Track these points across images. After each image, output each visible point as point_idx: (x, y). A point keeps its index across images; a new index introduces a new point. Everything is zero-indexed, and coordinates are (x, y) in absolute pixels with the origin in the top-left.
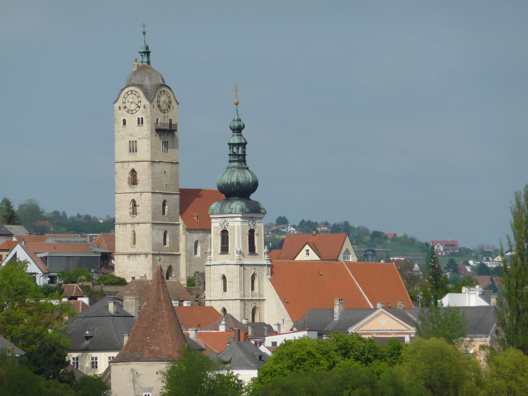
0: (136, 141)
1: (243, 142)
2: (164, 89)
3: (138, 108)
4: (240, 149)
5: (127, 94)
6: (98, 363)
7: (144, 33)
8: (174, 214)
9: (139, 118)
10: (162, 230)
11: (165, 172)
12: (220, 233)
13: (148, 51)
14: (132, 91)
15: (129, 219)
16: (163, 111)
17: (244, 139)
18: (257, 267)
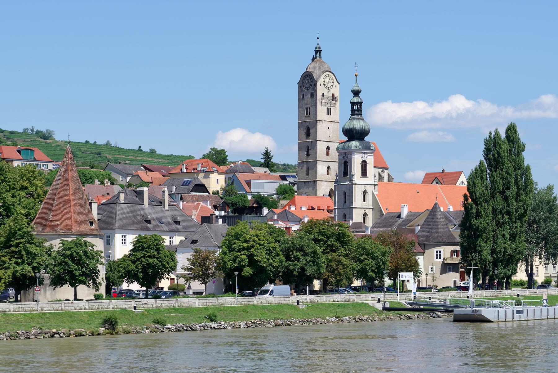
6: (121, 243)
7: (318, 39)
13: (320, 49)
14: (328, 75)
15: (325, 158)
17: (361, 99)
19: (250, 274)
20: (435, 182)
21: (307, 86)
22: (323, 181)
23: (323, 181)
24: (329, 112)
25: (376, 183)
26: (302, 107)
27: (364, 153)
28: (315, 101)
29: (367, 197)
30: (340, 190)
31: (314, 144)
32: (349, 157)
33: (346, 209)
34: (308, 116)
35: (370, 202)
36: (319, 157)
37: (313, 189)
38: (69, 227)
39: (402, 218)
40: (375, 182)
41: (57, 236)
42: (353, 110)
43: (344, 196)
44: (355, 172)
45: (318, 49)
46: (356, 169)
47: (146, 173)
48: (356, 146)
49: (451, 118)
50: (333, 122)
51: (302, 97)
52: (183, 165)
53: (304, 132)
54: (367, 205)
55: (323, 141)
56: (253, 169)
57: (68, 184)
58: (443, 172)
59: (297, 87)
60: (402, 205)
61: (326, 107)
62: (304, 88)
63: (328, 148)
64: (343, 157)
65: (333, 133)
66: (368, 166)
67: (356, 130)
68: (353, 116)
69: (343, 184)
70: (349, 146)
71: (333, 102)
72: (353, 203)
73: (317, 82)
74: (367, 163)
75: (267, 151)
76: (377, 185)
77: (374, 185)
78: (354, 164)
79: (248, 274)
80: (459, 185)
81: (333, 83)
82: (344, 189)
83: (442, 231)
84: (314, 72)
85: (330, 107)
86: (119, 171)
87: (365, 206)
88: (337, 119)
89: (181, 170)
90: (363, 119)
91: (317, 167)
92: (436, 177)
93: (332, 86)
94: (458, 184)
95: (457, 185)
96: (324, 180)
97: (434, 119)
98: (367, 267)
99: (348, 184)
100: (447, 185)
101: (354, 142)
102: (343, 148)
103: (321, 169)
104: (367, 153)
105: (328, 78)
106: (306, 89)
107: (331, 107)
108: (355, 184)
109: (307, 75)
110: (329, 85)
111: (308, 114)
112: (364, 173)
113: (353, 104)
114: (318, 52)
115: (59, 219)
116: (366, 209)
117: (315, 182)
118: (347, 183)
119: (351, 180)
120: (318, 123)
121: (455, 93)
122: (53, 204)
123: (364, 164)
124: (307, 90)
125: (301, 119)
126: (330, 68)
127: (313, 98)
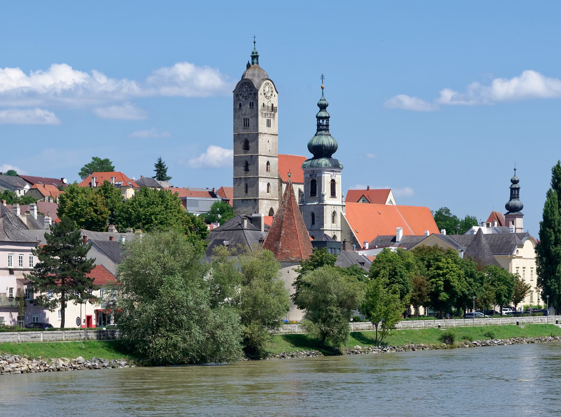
0: (248, 119)
1: (327, 116)
2: (269, 81)
3: (250, 95)
4: (325, 121)
5: (240, 89)
8: (274, 171)
9: (250, 103)
10: (266, 182)
11: (288, 272)
12: (310, 181)
13: (257, 55)
14: (268, 83)
16: (267, 97)
17: (328, 114)
18: (335, 207)
19: (446, 298)
20: (361, 201)
21: (245, 95)
22: (264, 199)
23: (264, 199)
24: (269, 124)
25: (344, 204)
26: (239, 117)
27: (333, 171)
28: (255, 112)
29: (335, 218)
30: (307, 210)
31: (255, 159)
32: (318, 175)
33: (315, 231)
34: (246, 128)
35: (338, 225)
36: (260, 173)
37: (254, 208)
38: (298, 255)
39: (397, 242)
40: (343, 203)
41: (290, 263)
42: (319, 125)
43: (311, 217)
44: (325, 191)
45: (255, 55)
46: (326, 189)
47: (44, 187)
48: (327, 164)
49: (55, 94)
50: (272, 135)
51: (238, 107)
52: (93, 178)
53: (241, 146)
54: (336, 226)
55: (264, 156)
56: (160, 184)
57: (292, 215)
58: (368, 189)
59: (232, 95)
60: (397, 228)
61: (266, 118)
62: (242, 96)
63: (268, 163)
64: (311, 175)
65: (273, 147)
66: (336, 186)
67: (325, 146)
68: (321, 132)
69: (310, 204)
70: (318, 164)
71: (273, 113)
72: (323, 225)
73: (258, 91)
74: (336, 182)
75: (160, 162)
76: (344, 206)
77: (342, 206)
78: (324, 183)
79: (445, 299)
80: (388, 204)
81: (272, 92)
82: (312, 210)
83: (488, 257)
84: (253, 80)
85: (269, 119)
86: (5, 184)
87: (334, 228)
88: (275, 132)
89: (90, 184)
90: (330, 135)
91: (258, 184)
92: (363, 195)
93: (272, 95)
94: (387, 203)
95: (386, 204)
96: (264, 198)
97: (31, 94)
98: (502, 292)
99: (317, 204)
100: (375, 204)
101: (323, 159)
102: (311, 166)
103: (262, 186)
104: (336, 171)
105: (268, 86)
106: (244, 98)
107: (271, 119)
108: (326, 205)
109: (246, 83)
110: (269, 95)
111: (246, 124)
112: (333, 194)
113: (319, 118)
114: (255, 58)
115: (288, 247)
116: (335, 231)
117: (256, 201)
118: (315, 203)
119: (321, 198)
120: (259, 136)
121: (60, 63)
122: (281, 233)
123: (333, 183)
124: (246, 99)
125: (237, 131)
126: (267, 75)
127: (253, 108)
